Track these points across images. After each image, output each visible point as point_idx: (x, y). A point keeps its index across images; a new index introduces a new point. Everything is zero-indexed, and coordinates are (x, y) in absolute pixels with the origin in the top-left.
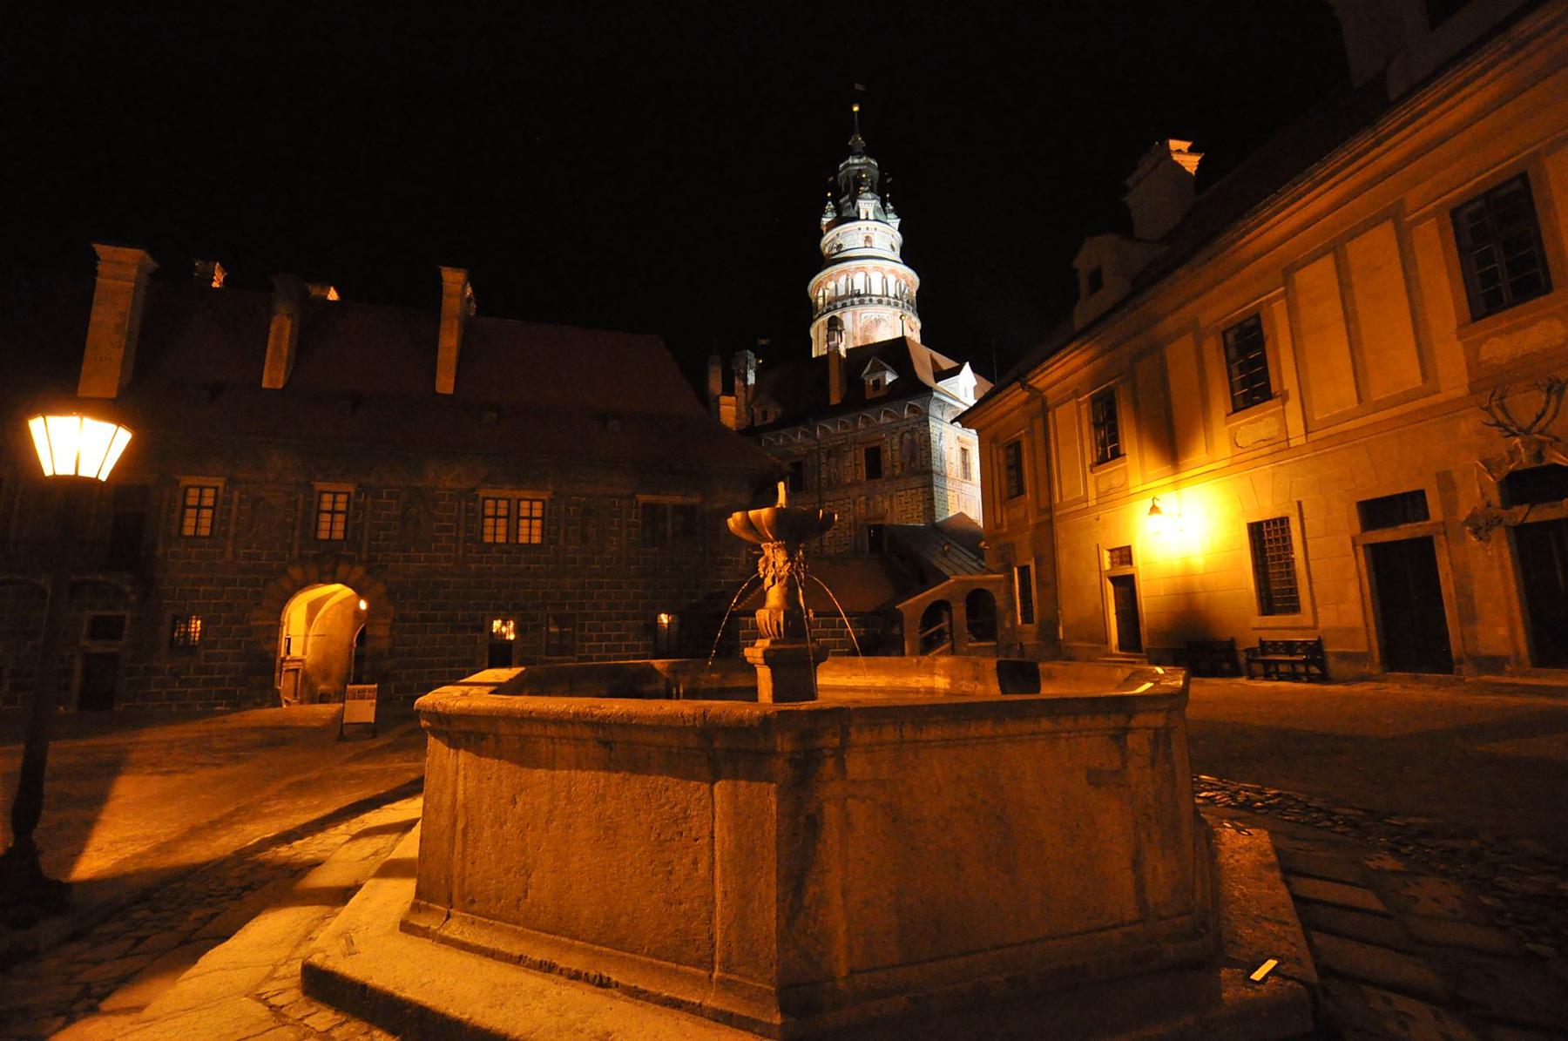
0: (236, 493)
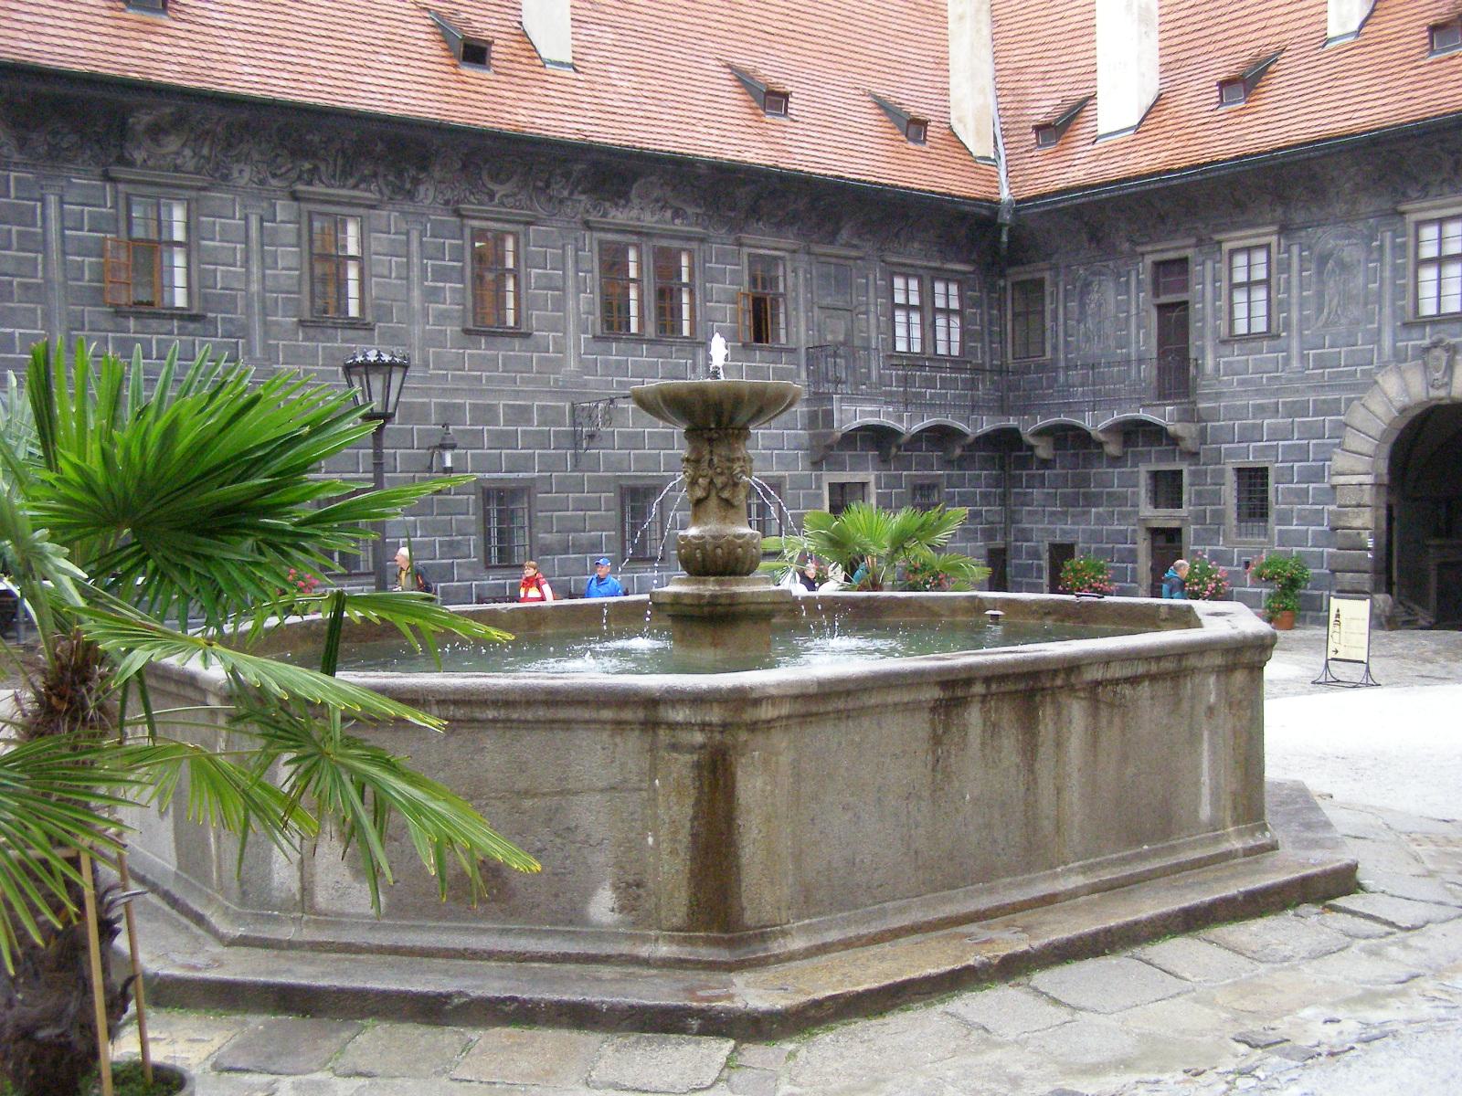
0: (1295, 249)
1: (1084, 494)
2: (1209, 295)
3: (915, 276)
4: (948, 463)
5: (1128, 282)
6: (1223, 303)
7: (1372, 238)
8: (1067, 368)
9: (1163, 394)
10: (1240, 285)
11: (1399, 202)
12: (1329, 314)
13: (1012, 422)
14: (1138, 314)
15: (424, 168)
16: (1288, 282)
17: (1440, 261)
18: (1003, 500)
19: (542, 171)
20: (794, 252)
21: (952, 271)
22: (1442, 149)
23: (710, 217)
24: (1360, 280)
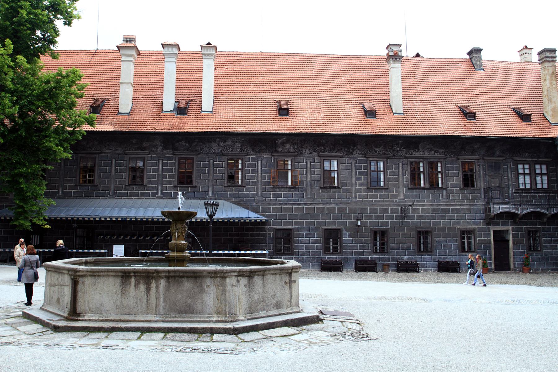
4: (541, 224)
15: (354, 146)
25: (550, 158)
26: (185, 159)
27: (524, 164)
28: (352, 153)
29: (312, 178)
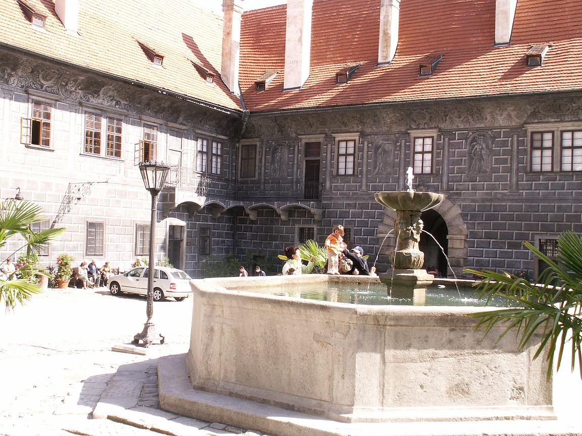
0: (366, 143)
1: (270, 235)
2: (329, 158)
3: (205, 139)
4: (213, 220)
5: (294, 150)
6: (335, 161)
7: (397, 142)
8: (265, 183)
9: (308, 197)
10: (342, 155)
11: (408, 129)
12: (379, 170)
13: (241, 204)
14: (297, 163)
15: (13, 70)
16: (362, 155)
17: (573, 148)
18: (233, 236)
19: (65, 78)
20: (161, 125)
21: (220, 138)
22: (427, 111)
23: (130, 106)
24: (392, 157)
25: (225, 136)
26: (532, 141)
27: (217, 143)
28: (7, 82)
29: (450, 179)
